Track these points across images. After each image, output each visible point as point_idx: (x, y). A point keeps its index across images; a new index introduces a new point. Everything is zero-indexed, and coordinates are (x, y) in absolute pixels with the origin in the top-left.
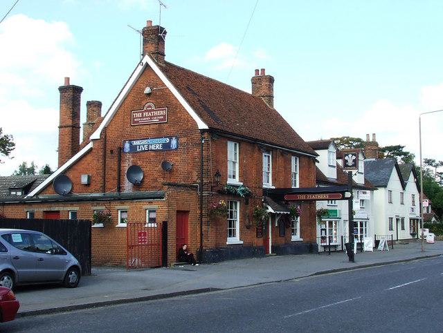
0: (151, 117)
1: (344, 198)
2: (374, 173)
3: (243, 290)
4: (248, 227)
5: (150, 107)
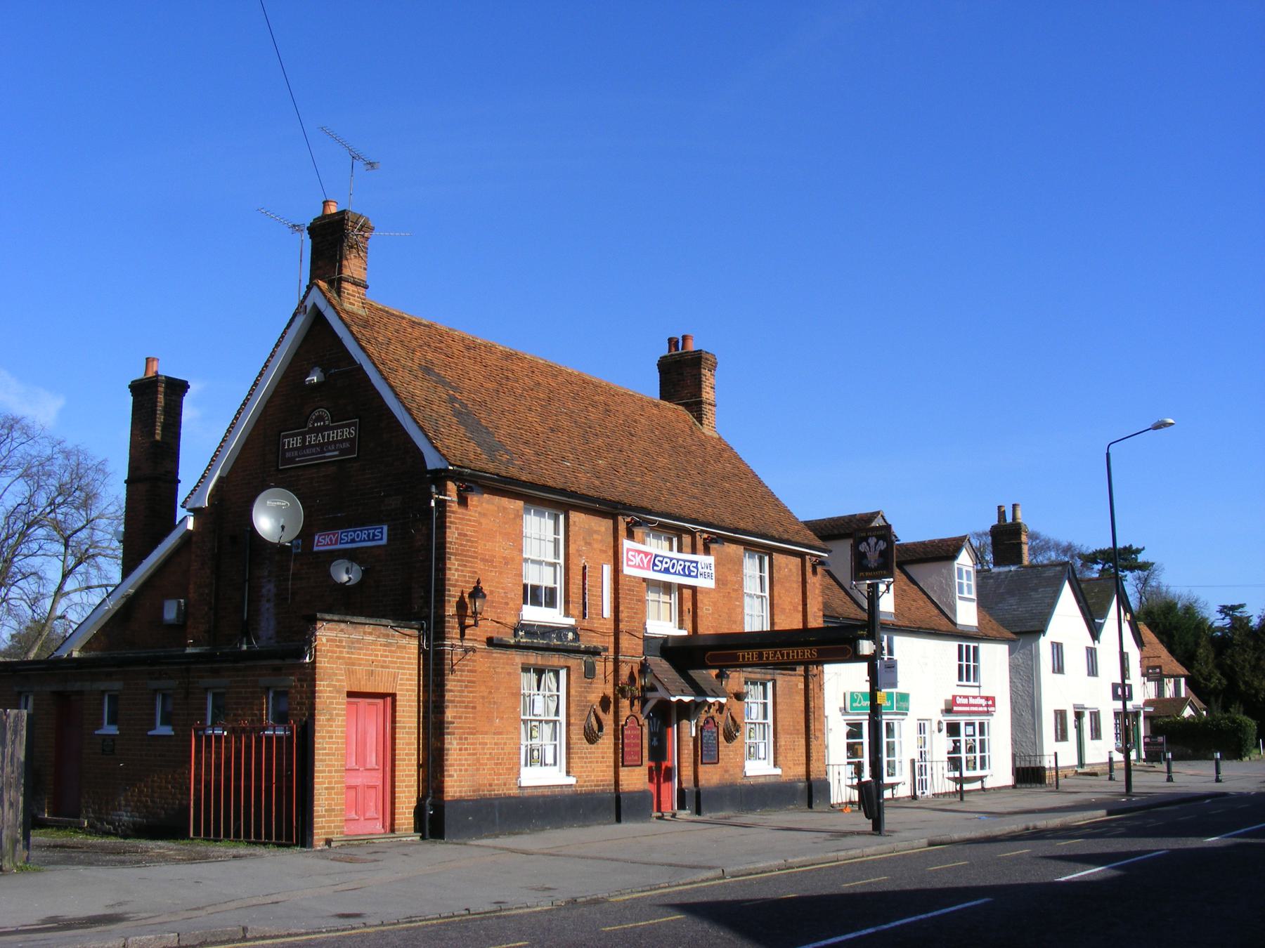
0: (321, 445)
1: (856, 657)
2: (1013, 601)
3: (768, 879)
4: (104, 740)
5: (320, 418)
